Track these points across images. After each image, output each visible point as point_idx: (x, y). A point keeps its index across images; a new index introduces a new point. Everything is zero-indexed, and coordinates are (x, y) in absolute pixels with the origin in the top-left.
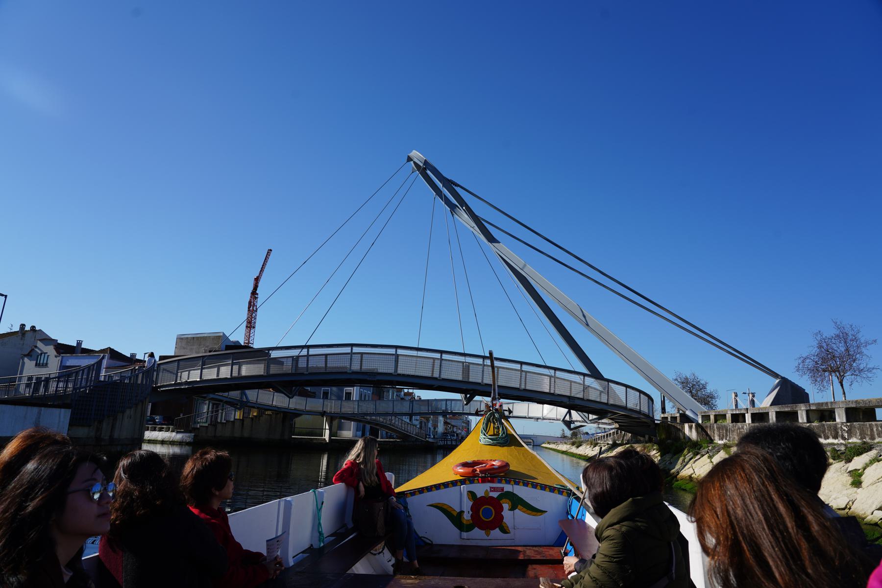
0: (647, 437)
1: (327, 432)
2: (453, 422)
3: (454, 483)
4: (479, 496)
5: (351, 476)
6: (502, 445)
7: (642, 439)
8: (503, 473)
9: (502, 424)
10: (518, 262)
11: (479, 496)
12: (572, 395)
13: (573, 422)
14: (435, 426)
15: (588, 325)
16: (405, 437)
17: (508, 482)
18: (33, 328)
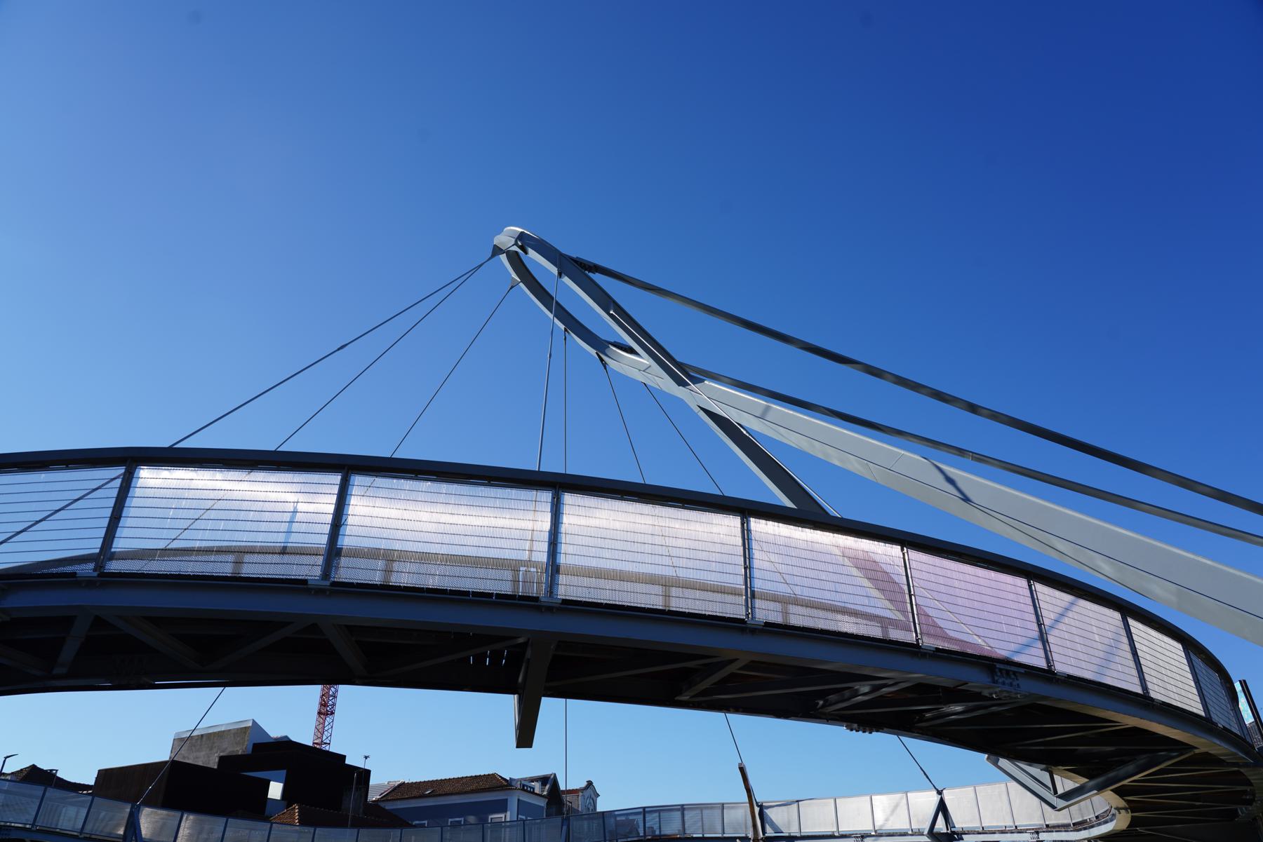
15: (966, 499)
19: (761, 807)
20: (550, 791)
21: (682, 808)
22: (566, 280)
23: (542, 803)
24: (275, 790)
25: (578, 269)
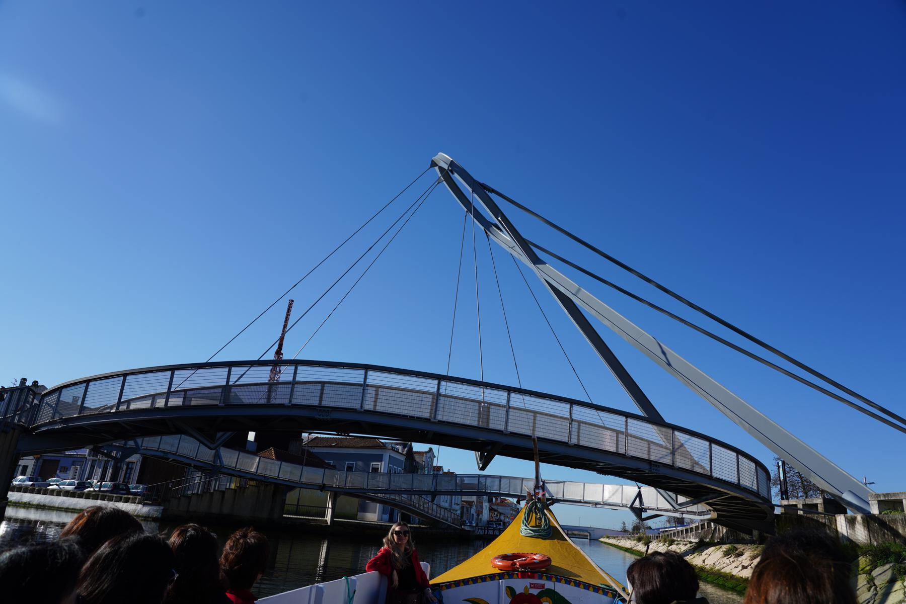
0: (755, 533)
1: (330, 512)
2: (500, 509)
3: (492, 577)
4: (518, 592)
5: (383, 565)
6: (544, 537)
7: (747, 537)
8: (543, 569)
9: (545, 515)
10: (568, 284)
11: (518, 592)
12: (653, 458)
13: (646, 510)
14: (479, 512)
15: (669, 364)
16: (434, 523)
17: (549, 579)
18: (35, 383)
19: (544, 482)
20: (408, 452)
21: (500, 478)
22: (475, 195)
23: (403, 458)
24: (251, 436)
25: (481, 189)
